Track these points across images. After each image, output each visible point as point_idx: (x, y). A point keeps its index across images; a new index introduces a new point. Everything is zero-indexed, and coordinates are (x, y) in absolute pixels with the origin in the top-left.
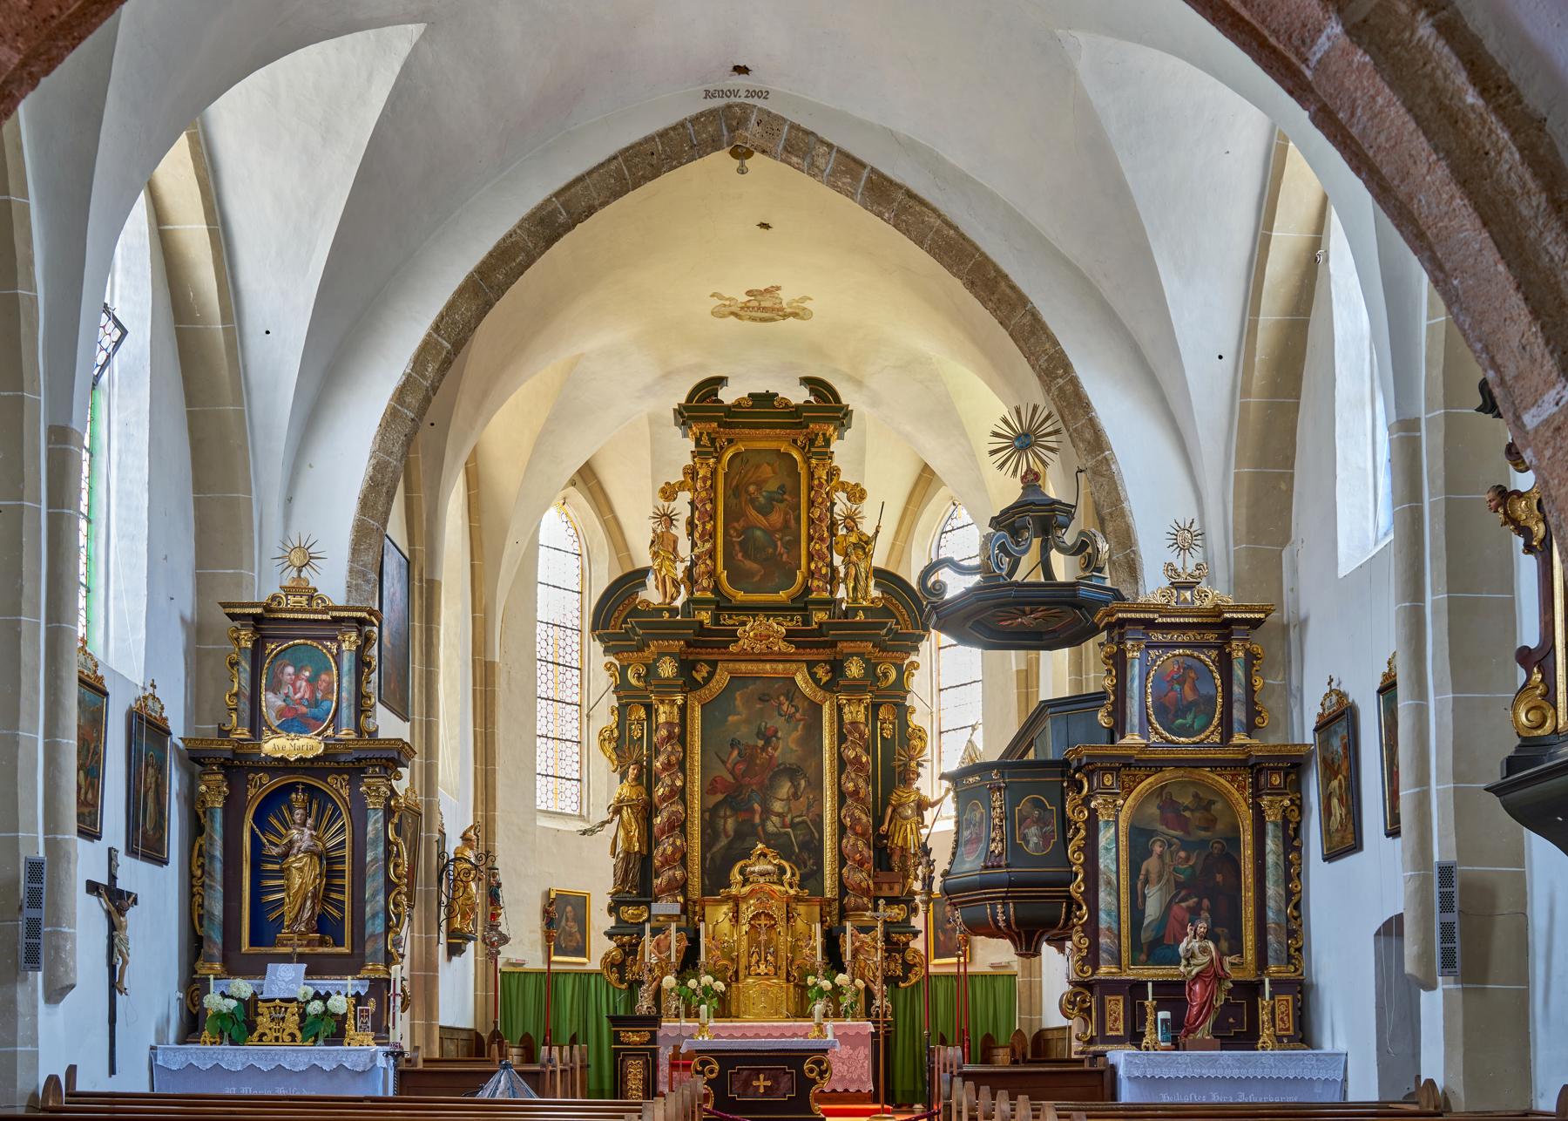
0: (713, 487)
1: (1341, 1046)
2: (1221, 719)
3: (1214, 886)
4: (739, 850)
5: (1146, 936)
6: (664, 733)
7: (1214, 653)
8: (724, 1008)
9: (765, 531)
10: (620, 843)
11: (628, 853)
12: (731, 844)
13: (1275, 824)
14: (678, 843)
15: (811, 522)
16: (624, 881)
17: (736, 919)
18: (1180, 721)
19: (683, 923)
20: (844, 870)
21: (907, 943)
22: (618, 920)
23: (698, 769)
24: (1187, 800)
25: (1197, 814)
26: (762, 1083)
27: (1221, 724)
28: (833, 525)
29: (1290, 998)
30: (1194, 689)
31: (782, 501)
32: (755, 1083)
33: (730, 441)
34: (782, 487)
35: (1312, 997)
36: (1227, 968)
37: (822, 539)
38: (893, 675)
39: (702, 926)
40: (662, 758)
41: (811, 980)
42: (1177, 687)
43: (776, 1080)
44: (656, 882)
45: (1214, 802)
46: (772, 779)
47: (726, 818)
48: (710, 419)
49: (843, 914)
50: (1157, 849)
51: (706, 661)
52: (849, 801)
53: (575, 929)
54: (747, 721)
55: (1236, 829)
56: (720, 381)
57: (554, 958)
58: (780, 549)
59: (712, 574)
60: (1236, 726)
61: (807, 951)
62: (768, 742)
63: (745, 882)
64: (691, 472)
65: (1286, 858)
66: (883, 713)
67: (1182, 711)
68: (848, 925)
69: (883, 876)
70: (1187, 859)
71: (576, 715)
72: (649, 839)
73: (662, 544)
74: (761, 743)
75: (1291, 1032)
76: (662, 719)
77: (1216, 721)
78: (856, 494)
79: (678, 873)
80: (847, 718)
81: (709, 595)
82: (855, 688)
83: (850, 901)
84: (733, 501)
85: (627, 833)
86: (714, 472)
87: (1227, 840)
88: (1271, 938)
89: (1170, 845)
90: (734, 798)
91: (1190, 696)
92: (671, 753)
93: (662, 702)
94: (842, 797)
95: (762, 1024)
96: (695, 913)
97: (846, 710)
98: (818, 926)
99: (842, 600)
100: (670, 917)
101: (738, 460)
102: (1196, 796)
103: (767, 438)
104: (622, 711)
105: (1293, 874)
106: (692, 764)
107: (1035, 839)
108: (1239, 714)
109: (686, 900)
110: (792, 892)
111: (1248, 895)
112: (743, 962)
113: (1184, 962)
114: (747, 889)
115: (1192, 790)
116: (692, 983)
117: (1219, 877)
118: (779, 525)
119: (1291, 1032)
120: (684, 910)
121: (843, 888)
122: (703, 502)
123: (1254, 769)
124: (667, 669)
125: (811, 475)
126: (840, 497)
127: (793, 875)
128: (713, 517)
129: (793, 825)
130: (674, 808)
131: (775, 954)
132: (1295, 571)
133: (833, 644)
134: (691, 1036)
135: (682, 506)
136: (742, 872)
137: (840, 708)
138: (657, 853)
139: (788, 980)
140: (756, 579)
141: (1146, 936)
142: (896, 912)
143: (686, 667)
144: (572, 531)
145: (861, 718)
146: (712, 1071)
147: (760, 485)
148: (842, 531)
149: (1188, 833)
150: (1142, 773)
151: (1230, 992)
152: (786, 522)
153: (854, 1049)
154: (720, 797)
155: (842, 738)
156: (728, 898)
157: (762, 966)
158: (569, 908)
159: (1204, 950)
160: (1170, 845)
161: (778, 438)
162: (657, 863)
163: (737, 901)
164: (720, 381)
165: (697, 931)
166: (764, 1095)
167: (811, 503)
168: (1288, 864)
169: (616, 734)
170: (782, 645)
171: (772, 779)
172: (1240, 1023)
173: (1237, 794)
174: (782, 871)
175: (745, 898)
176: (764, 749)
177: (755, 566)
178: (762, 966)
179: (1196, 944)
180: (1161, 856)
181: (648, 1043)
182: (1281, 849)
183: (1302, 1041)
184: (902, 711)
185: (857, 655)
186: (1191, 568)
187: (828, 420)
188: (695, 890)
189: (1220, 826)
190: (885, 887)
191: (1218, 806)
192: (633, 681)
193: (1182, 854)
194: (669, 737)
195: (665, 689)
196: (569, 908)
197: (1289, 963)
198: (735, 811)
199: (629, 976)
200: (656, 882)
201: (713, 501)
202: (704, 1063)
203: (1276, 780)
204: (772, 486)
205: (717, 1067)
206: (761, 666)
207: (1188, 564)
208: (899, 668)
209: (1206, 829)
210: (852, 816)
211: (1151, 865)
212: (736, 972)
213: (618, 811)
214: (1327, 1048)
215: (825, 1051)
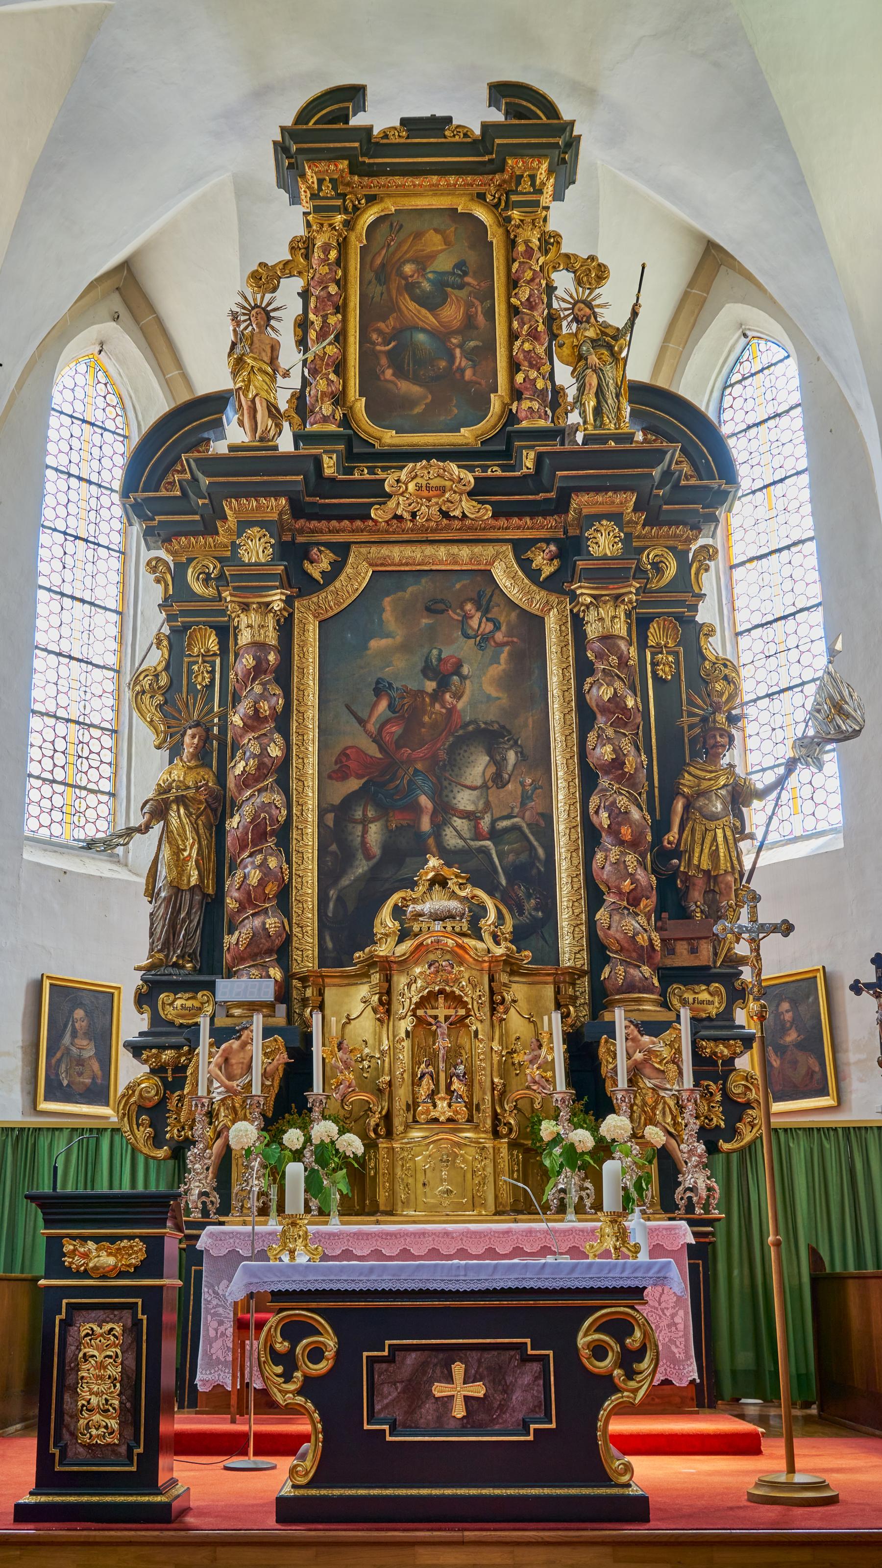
0: (341, 261)
4: (396, 866)
6: (248, 661)
8: (364, 1192)
9: (432, 333)
10: (163, 871)
11: (176, 890)
12: (374, 870)
14: (273, 863)
15: (513, 311)
16: (167, 945)
17: (385, 1007)
19: (280, 1019)
20: (601, 915)
21: (729, 1062)
22: (156, 1019)
23: (313, 734)
26: (458, 1389)
28: (552, 319)
31: (461, 287)
32: (440, 1390)
33: (372, 199)
34: (461, 265)
38: (671, 569)
39: (317, 1018)
40: (244, 707)
41: (547, 1129)
43: (496, 1377)
44: (230, 940)
46: (452, 751)
47: (365, 822)
48: (335, 155)
49: (601, 999)
51: (329, 545)
52: (604, 782)
53: (89, 1052)
54: (405, 648)
56: (354, 95)
57: (44, 1106)
59: (339, 398)
61: (533, 1072)
62: (443, 684)
63: (404, 935)
64: (303, 247)
66: (655, 634)
68: (619, 1016)
69: (675, 928)
71: (110, 686)
72: (219, 862)
73: (250, 343)
74: (430, 686)
76: (245, 637)
78: (592, 273)
79: (272, 922)
80: (592, 630)
81: (332, 428)
82: (607, 574)
83: (614, 973)
84: (376, 290)
85: (177, 852)
86: (343, 245)
90: (384, 797)
92: (262, 697)
93: (245, 607)
94: (588, 778)
95: (447, 1233)
96: (304, 1002)
97: (591, 616)
98: (556, 1017)
99: (575, 428)
100: (253, 1007)
101: (384, 227)
103: (435, 190)
104: (177, 639)
106: (302, 724)
109: (289, 976)
110: (499, 951)
112: (402, 1094)
114: (406, 947)
116: (293, 1137)
118: (456, 324)
120: (283, 994)
121: (598, 950)
122: (323, 284)
124: (256, 549)
125: (511, 244)
126: (563, 281)
127: (500, 916)
128: (341, 309)
129: (494, 835)
130: (265, 798)
131: (468, 1078)
133: (561, 505)
134: (262, 1255)
135: (288, 298)
136: (398, 912)
137: (578, 623)
138: (232, 885)
139: (496, 1134)
140: (418, 410)
142: (709, 999)
143: (292, 553)
144: (112, 399)
145: (620, 628)
146: (316, 1355)
147: (422, 262)
148: (567, 328)
152: (469, 323)
154: (354, 784)
155: (583, 669)
156: (371, 963)
157: (442, 1105)
158: (79, 1013)
161: (451, 190)
162: (231, 904)
163: (387, 968)
164: (354, 95)
165: (308, 1038)
166: (469, 1423)
167: (513, 283)
169: (164, 680)
170: (467, 506)
171: (452, 751)
174: (477, 912)
175: (404, 964)
176: (436, 696)
177: (416, 390)
178: (442, 1105)
181: (140, 1271)
184: (691, 633)
185: (609, 517)
187: (537, 151)
188: (306, 954)
190: (682, 948)
192: (198, 588)
194: (259, 670)
195: (249, 582)
196: (79, 1013)
198: (384, 811)
199: (172, 1132)
200: (230, 940)
201: (343, 284)
202: (295, 1331)
204: (444, 264)
205: (330, 1342)
206: (429, 550)
208: (681, 556)
210: (612, 808)
212: (388, 1118)
213: (159, 810)
215: (637, 1293)
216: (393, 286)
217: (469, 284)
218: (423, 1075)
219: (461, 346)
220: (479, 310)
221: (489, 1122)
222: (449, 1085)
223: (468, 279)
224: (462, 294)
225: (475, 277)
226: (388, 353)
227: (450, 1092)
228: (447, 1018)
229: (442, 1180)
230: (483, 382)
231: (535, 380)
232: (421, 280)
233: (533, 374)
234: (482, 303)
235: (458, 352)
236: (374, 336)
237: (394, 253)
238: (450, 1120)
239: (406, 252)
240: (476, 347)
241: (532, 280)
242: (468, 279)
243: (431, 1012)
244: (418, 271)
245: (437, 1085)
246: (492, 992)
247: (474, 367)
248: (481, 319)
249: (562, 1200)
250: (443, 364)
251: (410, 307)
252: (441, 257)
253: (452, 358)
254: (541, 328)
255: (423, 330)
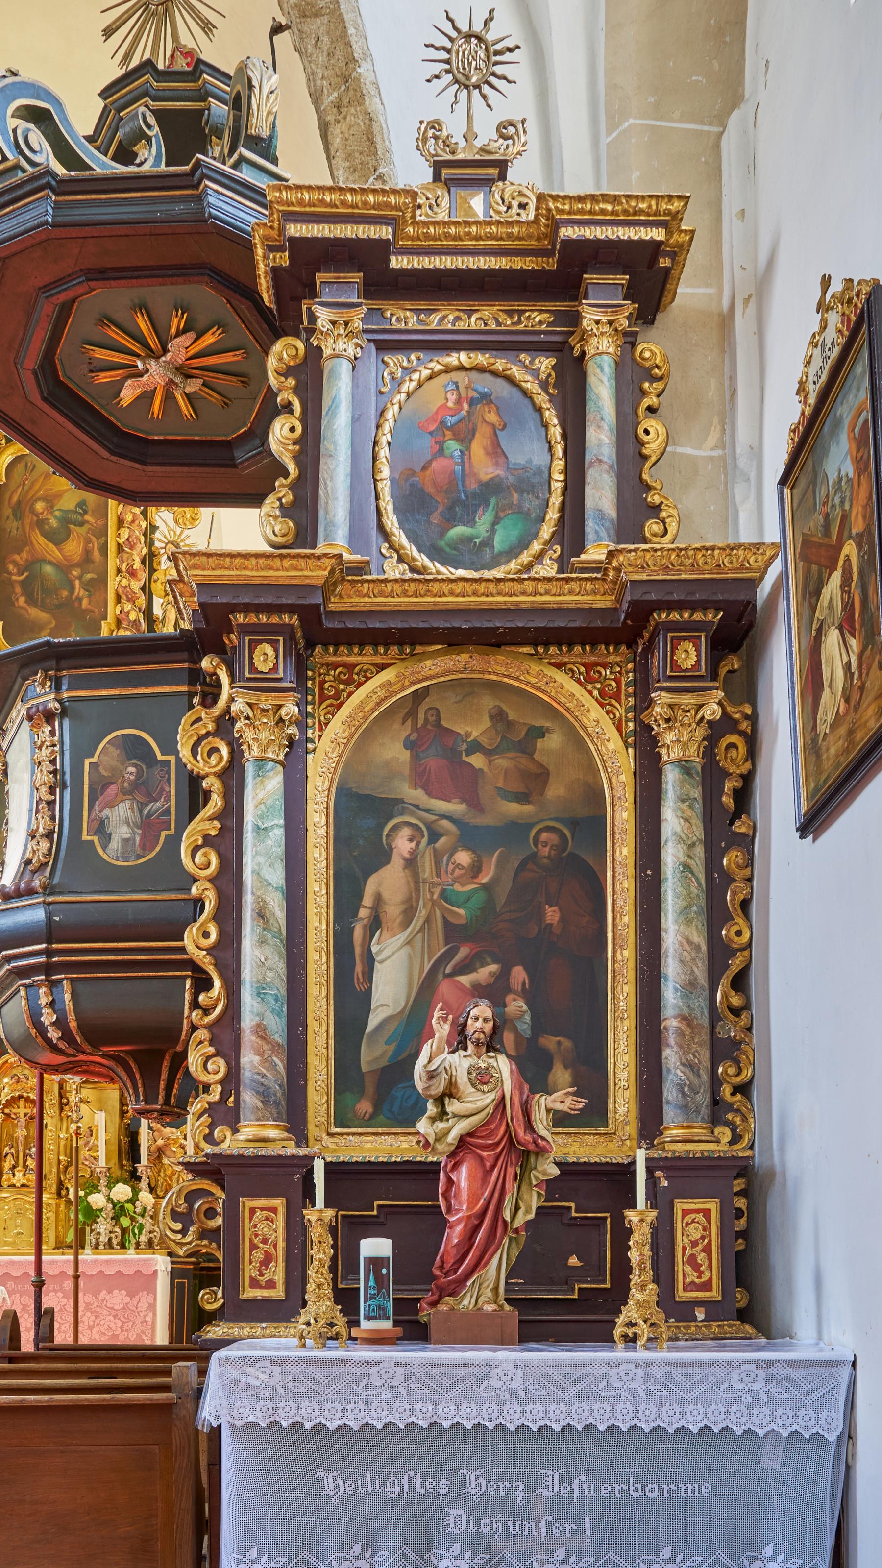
1: (841, 1341)
2: (561, 520)
3: (539, 943)
5: (371, 1055)
7: (545, 364)
9: (57, 566)
13: (685, 768)
18: (458, 531)
24: (475, 728)
25: (502, 762)
27: (558, 536)
29: (713, 1206)
30: (496, 451)
31: (81, 524)
35: (773, 1204)
36: (542, 1124)
37: (132, 574)
42: (453, 447)
45: (541, 733)
50: (403, 845)
55: (594, 796)
58: (79, 591)
60: (590, 526)
65: (712, 862)
67: (462, 508)
70: (476, 869)
75: (715, 1294)
77: (546, 531)
87: (574, 823)
88: (671, 1056)
89: (434, 836)
91: (486, 469)
101: (20, 467)
102: (498, 716)
105: (727, 901)
107: (124, 832)
108: (601, 495)
111: (621, 958)
113: (432, 1109)
115: (488, 702)
117: (552, 915)
118: (77, 558)
119: (715, 1294)
123: (623, 632)
132: (751, 166)
141: (371, 1055)
147: (51, 500)
149: (475, 804)
150: (366, 657)
151: (551, 1185)
152: (87, 553)
153: (131, 1295)
157: (19, 1174)
159: (482, 1078)
160: (434, 836)
168: (716, 882)
172: (594, 1269)
173: (596, 712)
179: (461, 1063)
180: (411, 863)
182: (698, 831)
183: (743, 1315)
186: (486, 134)
189: (555, 791)
191: (554, 741)
193: (464, 857)
197: (715, 1119)
203: (689, 656)
207: (474, 125)
209: (522, 798)
211: (388, 883)
214: (805, 1343)
216: (27, 521)
217: (88, 522)
218: (7, 1155)
219: (80, 578)
220: (95, 545)
221: (55, 1186)
222: (25, 1161)
223: (87, 517)
224: (82, 530)
225: (92, 516)
226: (23, 583)
227: (25, 1166)
228: (25, 1115)
229: (16, 1226)
230: (96, 610)
231: (128, 612)
232: (49, 517)
233: (128, 607)
234: (98, 539)
235: (77, 583)
236: (11, 567)
237: (28, 492)
238: (23, 1186)
239: (39, 490)
240: (92, 579)
241: (133, 521)
242: (87, 517)
243: (14, 1111)
244: (46, 509)
245: (17, 1161)
246: (61, 1096)
247: (89, 597)
248: (96, 554)
249: (97, 1239)
250: (65, 593)
251: (40, 541)
252: (66, 496)
253: (73, 588)
254: (137, 565)
255: (50, 563)
